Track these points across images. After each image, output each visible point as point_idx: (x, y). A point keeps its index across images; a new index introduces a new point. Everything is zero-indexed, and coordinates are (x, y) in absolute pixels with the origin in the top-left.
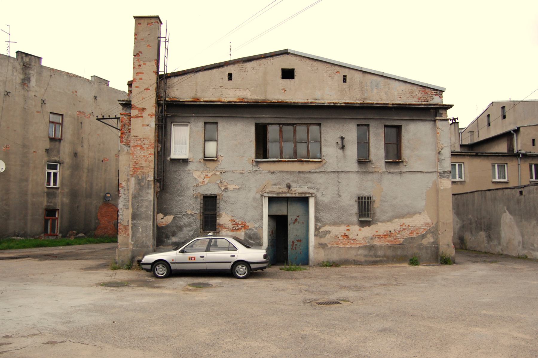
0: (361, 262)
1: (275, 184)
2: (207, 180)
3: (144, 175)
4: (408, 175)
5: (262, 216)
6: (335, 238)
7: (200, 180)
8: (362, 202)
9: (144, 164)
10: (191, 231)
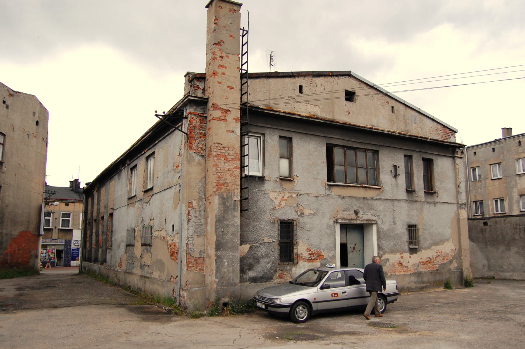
0: (413, 289)
1: (345, 210)
2: (283, 203)
3: (229, 193)
5: (335, 244)
6: (393, 266)
7: (277, 202)
8: (411, 230)
9: (229, 179)
10: (269, 263)
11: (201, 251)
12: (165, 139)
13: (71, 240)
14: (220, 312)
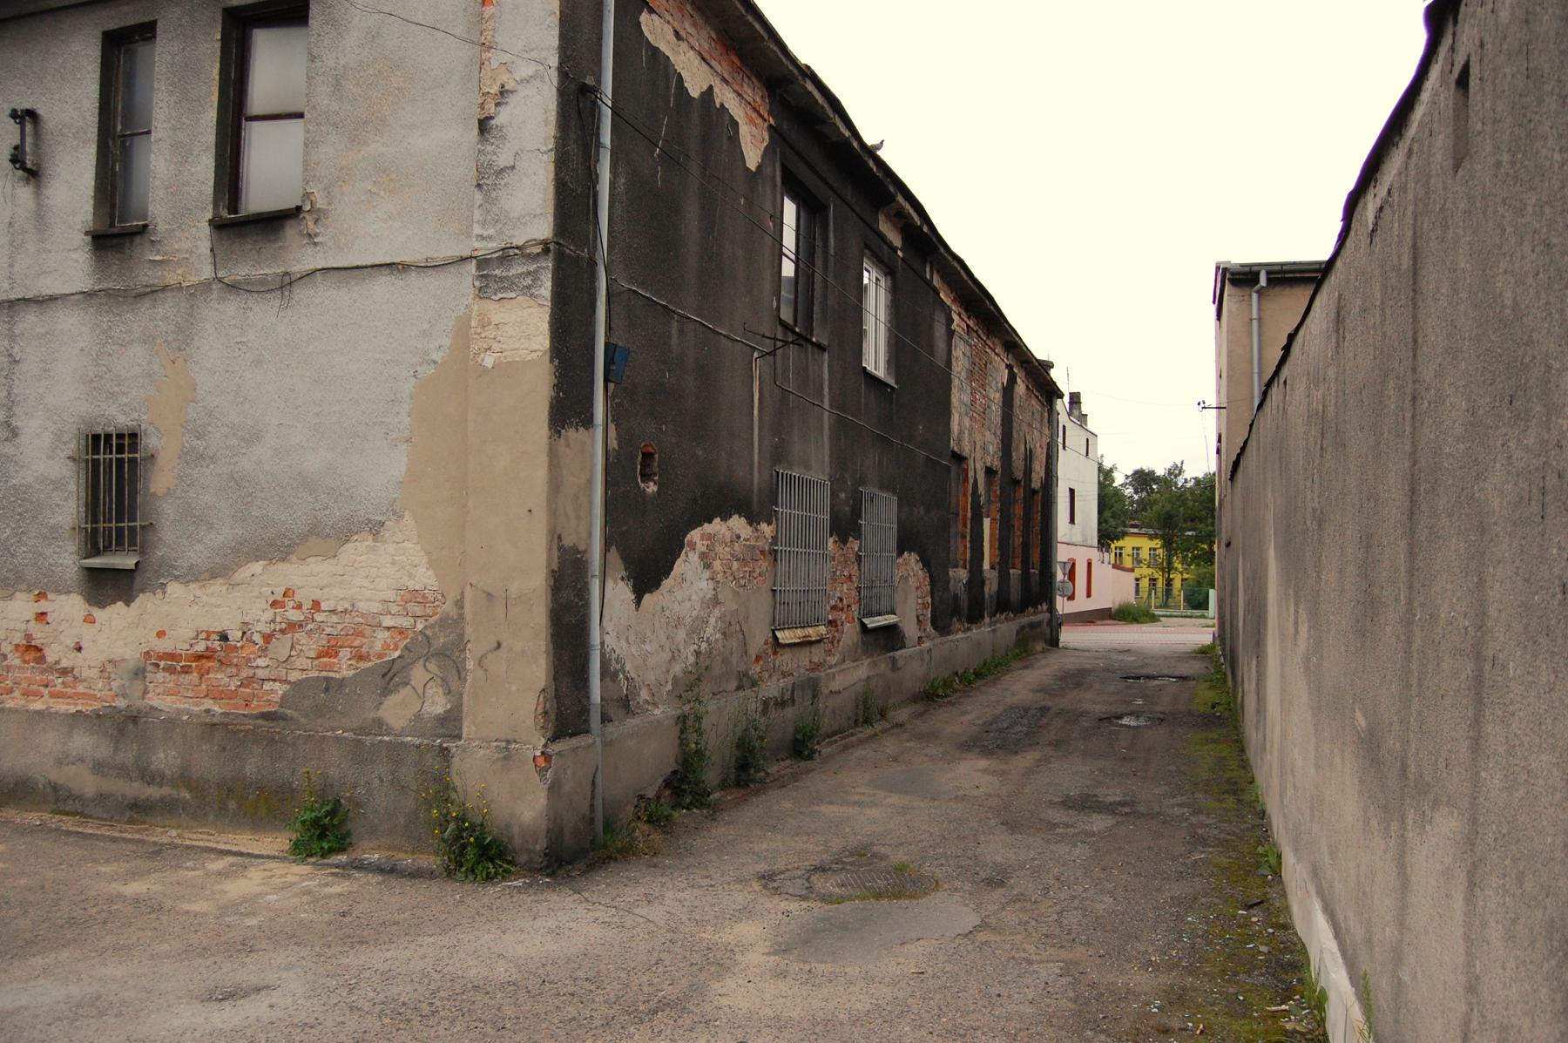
4: (324, 295)
8: (111, 459)
14: (1450, 482)
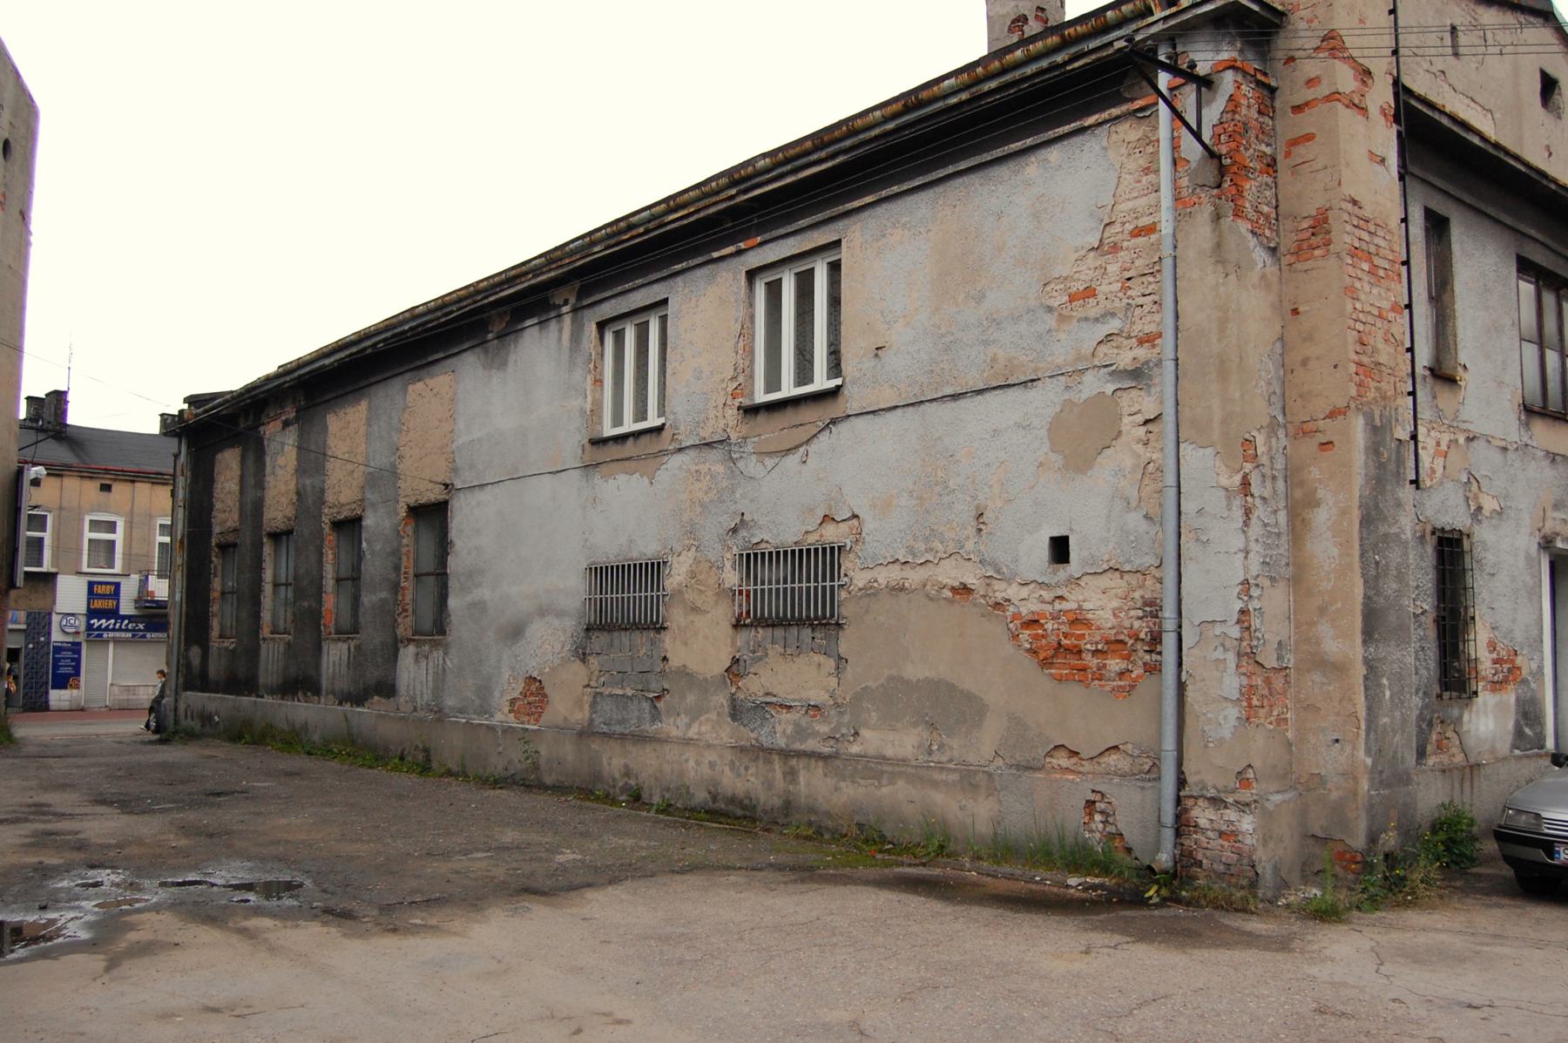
11: (1280, 643)
12: (939, 189)
13: (50, 614)
